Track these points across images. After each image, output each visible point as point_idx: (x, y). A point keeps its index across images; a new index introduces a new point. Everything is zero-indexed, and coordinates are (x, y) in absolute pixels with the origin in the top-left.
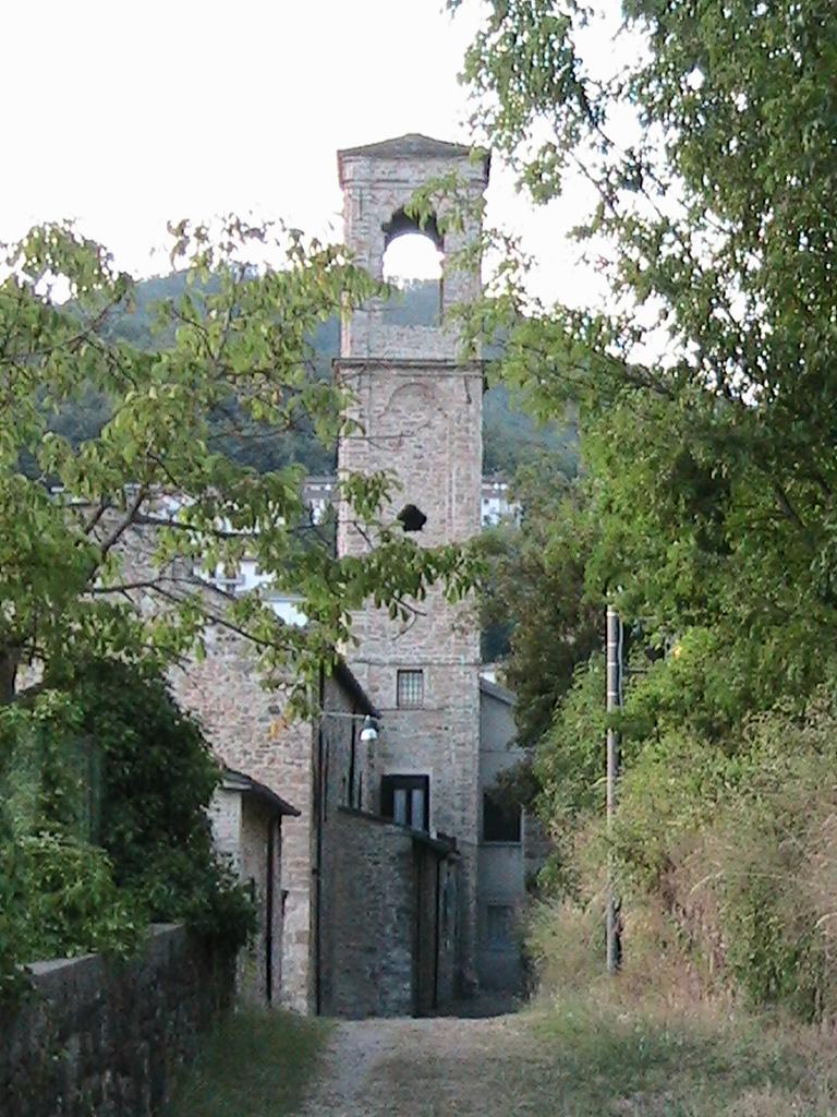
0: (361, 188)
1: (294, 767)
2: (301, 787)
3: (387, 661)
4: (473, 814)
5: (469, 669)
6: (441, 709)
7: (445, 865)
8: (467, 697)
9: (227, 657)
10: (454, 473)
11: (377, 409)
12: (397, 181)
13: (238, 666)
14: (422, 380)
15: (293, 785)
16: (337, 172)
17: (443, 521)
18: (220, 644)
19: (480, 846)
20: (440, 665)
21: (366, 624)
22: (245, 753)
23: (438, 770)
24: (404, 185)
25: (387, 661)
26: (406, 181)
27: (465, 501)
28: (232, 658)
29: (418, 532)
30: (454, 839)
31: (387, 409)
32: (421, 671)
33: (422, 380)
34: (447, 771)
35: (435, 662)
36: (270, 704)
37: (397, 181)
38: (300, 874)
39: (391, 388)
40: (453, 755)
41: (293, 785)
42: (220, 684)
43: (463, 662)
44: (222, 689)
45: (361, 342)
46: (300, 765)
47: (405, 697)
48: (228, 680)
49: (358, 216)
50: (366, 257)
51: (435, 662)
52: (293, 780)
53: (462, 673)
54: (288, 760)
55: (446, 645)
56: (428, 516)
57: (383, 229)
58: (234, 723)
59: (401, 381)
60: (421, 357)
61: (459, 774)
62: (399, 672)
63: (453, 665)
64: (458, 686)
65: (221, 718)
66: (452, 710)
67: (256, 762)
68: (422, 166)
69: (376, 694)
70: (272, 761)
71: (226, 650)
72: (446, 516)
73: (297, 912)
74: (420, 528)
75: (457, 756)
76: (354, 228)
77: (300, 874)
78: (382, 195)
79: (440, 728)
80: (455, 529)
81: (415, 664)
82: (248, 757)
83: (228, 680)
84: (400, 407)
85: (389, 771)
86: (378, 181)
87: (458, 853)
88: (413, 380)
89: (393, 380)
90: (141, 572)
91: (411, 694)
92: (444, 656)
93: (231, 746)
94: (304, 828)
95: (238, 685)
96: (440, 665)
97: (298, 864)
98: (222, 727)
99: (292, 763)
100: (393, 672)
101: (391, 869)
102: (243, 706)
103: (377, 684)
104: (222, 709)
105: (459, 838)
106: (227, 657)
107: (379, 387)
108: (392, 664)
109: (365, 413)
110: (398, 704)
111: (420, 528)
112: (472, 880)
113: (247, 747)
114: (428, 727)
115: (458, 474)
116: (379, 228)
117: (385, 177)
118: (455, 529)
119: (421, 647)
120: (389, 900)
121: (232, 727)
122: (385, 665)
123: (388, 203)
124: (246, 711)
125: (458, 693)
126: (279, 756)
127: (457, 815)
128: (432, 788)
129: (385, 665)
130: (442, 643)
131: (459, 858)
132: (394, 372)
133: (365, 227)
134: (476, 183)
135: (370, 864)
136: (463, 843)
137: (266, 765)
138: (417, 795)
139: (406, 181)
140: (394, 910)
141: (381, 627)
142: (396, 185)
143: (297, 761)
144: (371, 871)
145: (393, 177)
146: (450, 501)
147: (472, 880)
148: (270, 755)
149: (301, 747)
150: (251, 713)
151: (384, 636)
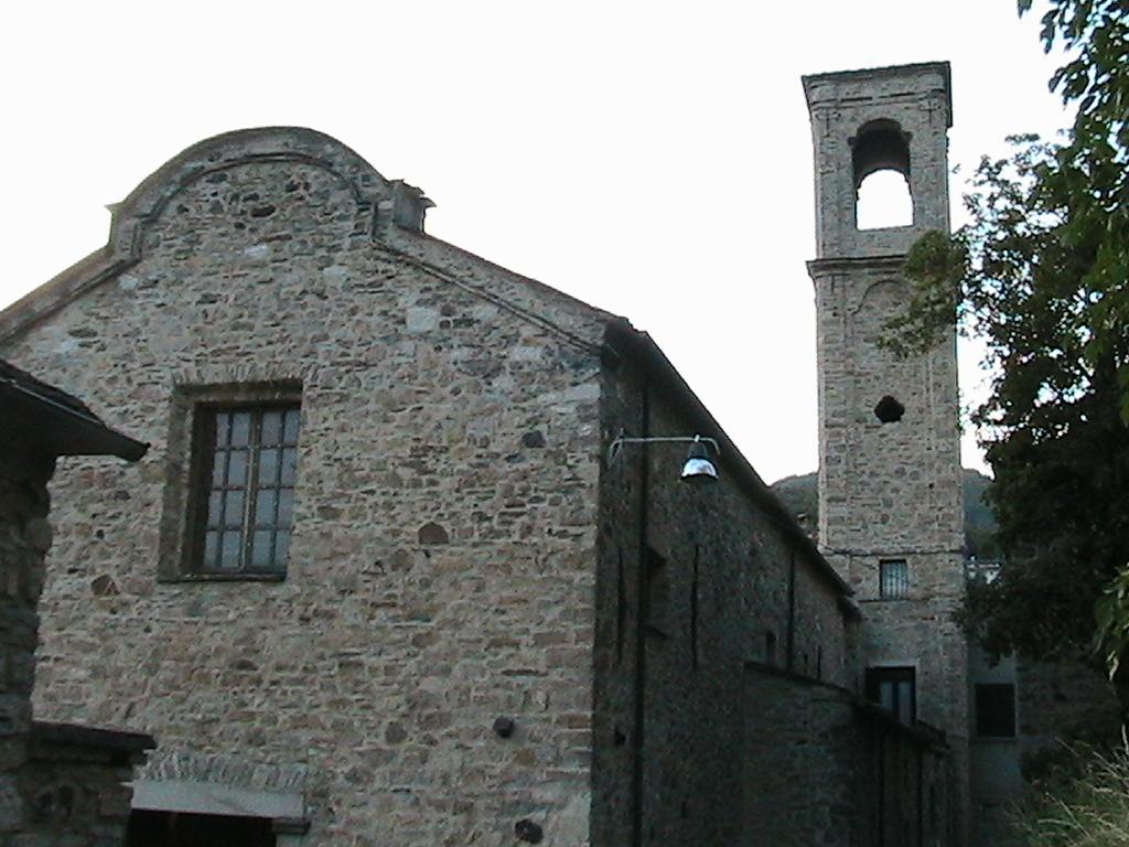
0: (828, 108)
1: (567, 541)
2: (577, 576)
3: (869, 552)
4: (963, 705)
5: (953, 556)
6: (925, 599)
7: (929, 759)
8: (954, 585)
9: (456, 354)
10: (930, 362)
11: (850, 306)
12: (860, 99)
13: (472, 367)
14: (894, 277)
15: (564, 574)
16: (805, 100)
17: (921, 411)
18: (446, 333)
19: (972, 742)
20: (922, 553)
21: (846, 516)
22: (482, 517)
23: (924, 662)
24: (868, 102)
25: (869, 552)
26: (870, 98)
27: (943, 388)
28: (465, 353)
29: (897, 423)
30: (944, 733)
31: (860, 307)
32: (904, 561)
33: (894, 277)
34: (935, 663)
35: (918, 550)
36: (526, 430)
37: (860, 99)
38: (573, 741)
39: (863, 285)
40: (941, 647)
41: (564, 574)
42: (443, 399)
43: (947, 549)
44: (446, 408)
45: (832, 245)
46: (577, 537)
47: (889, 588)
48: (456, 392)
49: (825, 133)
50: (834, 168)
51: (918, 550)
52: (563, 564)
53: (947, 561)
54: (556, 528)
55: (929, 533)
56: (907, 405)
57: (850, 143)
58: (463, 466)
59: (874, 279)
60: (890, 254)
61: (946, 666)
62: (882, 562)
63: (938, 552)
64: (943, 574)
65: (443, 457)
66: (937, 599)
67: (499, 535)
68: (884, 85)
69: (859, 586)
70: (528, 530)
71: (455, 341)
72: (924, 406)
73: (569, 812)
74: (899, 419)
75: (945, 647)
76: (821, 144)
77: (573, 741)
78: (846, 114)
79: (925, 619)
80: (934, 416)
81: (897, 554)
82: (486, 524)
83: (456, 392)
84: (873, 304)
85: (874, 664)
86: (843, 100)
87: (948, 747)
88: (885, 277)
89: (865, 279)
90: (325, 228)
91: (894, 586)
92: (928, 544)
93: (457, 507)
94: (582, 653)
95: (473, 398)
96: (922, 553)
97: (571, 721)
98: (443, 474)
99: (563, 534)
100: (874, 562)
101: (823, 749)
102: (480, 434)
103: (859, 575)
104: (445, 443)
105: (949, 733)
106: (456, 354)
107: (852, 286)
108: (874, 554)
109: (839, 311)
110: (881, 594)
111: (899, 419)
112: (965, 776)
113: (484, 507)
114: (913, 618)
115: (933, 363)
116: (845, 143)
117: (849, 97)
118: (934, 416)
119: (902, 536)
120: (820, 794)
121: (459, 472)
122: (867, 555)
123: (853, 119)
124: (486, 443)
125: (943, 581)
126: (540, 522)
127: (946, 708)
128: (919, 680)
129: (867, 555)
130: (925, 531)
131: (948, 752)
132: (866, 270)
133: (833, 143)
134: (936, 93)
135: (791, 744)
136: (954, 737)
137: (516, 538)
138: (904, 688)
139: (870, 98)
140: (827, 809)
141: (862, 518)
142: (859, 103)
143: (573, 530)
144: (794, 754)
145: (857, 96)
146: (928, 390)
147: (965, 776)
148: (525, 518)
149: (580, 501)
150: (493, 448)
151: (865, 527)
